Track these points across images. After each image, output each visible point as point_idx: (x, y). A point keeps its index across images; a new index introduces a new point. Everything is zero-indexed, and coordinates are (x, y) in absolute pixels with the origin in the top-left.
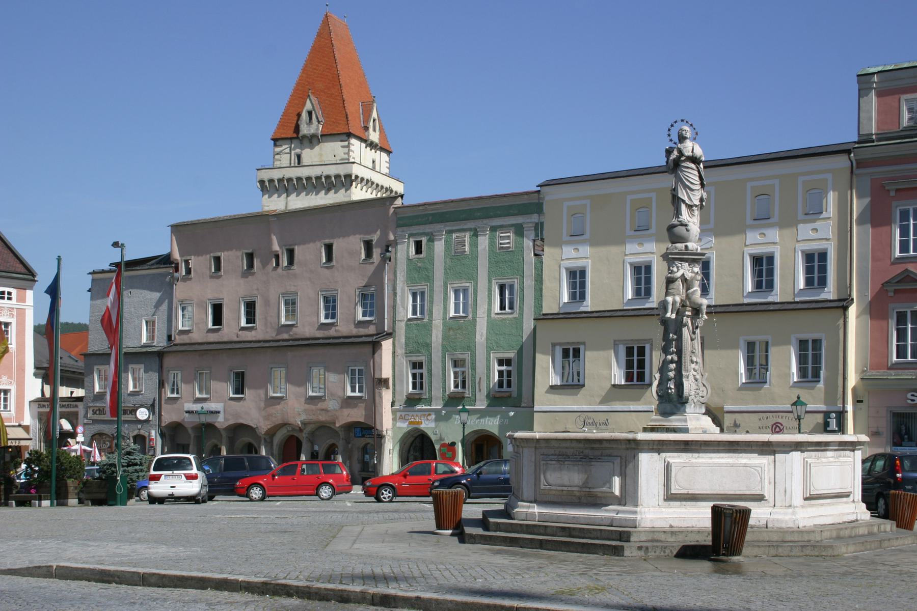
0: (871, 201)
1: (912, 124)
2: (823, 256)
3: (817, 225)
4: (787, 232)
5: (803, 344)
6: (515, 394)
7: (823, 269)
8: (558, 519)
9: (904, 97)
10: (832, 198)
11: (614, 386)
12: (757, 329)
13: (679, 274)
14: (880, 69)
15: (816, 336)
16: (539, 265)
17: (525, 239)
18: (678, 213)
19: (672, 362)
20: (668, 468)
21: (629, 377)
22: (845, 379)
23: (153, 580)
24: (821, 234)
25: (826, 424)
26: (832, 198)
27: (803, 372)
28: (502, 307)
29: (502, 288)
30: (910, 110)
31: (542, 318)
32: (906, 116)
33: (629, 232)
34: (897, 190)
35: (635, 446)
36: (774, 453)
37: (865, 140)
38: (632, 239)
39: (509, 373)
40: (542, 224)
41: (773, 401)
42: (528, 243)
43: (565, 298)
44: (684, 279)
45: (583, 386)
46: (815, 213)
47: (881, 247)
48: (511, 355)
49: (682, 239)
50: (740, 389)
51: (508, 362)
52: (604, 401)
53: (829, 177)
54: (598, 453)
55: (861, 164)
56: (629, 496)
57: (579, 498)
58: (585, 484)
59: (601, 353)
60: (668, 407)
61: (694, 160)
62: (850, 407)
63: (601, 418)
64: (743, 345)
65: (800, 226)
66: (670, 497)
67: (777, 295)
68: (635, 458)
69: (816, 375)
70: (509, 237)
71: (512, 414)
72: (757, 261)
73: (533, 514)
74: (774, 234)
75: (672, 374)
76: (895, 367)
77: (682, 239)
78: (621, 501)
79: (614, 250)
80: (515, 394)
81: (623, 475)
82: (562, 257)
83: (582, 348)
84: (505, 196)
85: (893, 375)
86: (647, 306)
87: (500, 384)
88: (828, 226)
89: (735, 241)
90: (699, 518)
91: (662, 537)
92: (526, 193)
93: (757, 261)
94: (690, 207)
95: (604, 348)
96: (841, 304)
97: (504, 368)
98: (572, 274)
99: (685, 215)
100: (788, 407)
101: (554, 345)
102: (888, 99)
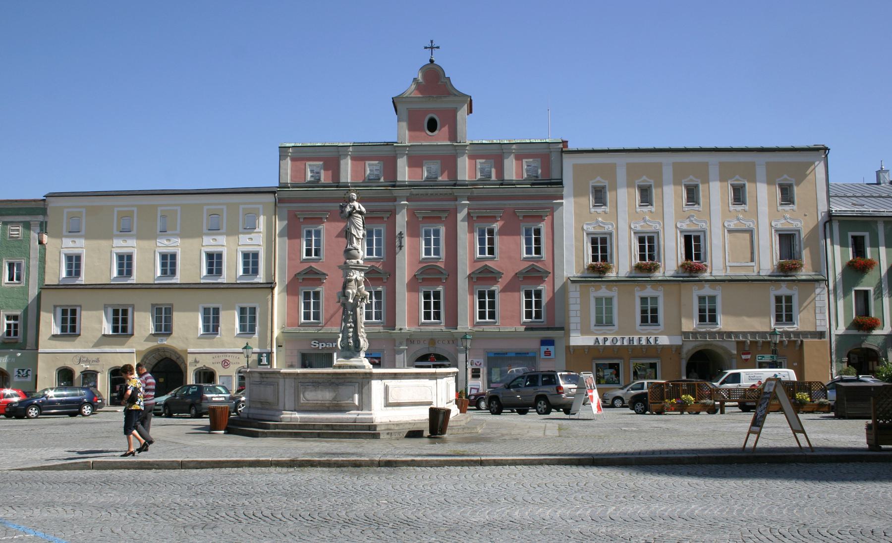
0: (288, 224)
1: (312, 179)
2: (256, 255)
3: (252, 236)
4: (232, 239)
5: (242, 311)
6: (21, 341)
7: (256, 264)
8: (322, 420)
9: (308, 163)
10: (262, 220)
11: (104, 335)
12: (212, 300)
13: (354, 277)
14: (293, 145)
15: (252, 305)
16: (42, 251)
17: (32, 232)
18: (351, 243)
19: (351, 327)
20: (386, 389)
21: (115, 329)
22: (272, 332)
23: (191, 465)
24: (256, 241)
25: (260, 361)
26: (262, 220)
27: (243, 328)
28: (11, 279)
29: (11, 266)
30: (312, 171)
31: (45, 288)
32: (309, 174)
33: (115, 232)
34: (305, 218)
35: (370, 376)
36: (436, 379)
37: (283, 186)
38: (118, 237)
39: (16, 326)
40: (46, 222)
41: (223, 346)
42: (34, 235)
43: (64, 274)
44: (356, 280)
45: (79, 335)
46: (250, 228)
47: (293, 253)
48: (18, 312)
49: (355, 257)
50: (199, 338)
51: (15, 318)
52: (95, 346)
53: (261, 207)
54: (340, 381)
55: (281, 201)
56: (365, 404)
57: (328, 407)
58: (334, 399)
59: (94, 312)
60: (348, 353)
61: (361, 213)
62: (274, 350)
63: (94, 357)
64: (201, 310)
65: (241, 236)
66: (388, 405)
67: (224, 279)
68: (369, 383)
69: (252, 330)
70: (18, 230)
71: (19, 354)
72: (210, 256)
73: (296, 418)
74: (222, 240)
75: (351, 334)
76: (303, 325)
77: (355, 257)
78: (360, 408)
79: (104, 243)
80: (21, 341)
81: (361, 394)
82: (59, 248)
83: (78, 310)
84: (16, 201)
85: (302, 330)
86: (129, 282)
87: (8, 333)
88: (259, 235)
89: (193, 242)
90: (422, 415)
91: (392, 427)
92: (35, 201)
93: (210, 256)
94: (358, 239)
95: (97, 309)
96: (269, 286)
97: (12, 322)
98: (69, 258)
99: (355, 244)
100: (240, 350)
101: (55, 307)
102: (298, 163)
